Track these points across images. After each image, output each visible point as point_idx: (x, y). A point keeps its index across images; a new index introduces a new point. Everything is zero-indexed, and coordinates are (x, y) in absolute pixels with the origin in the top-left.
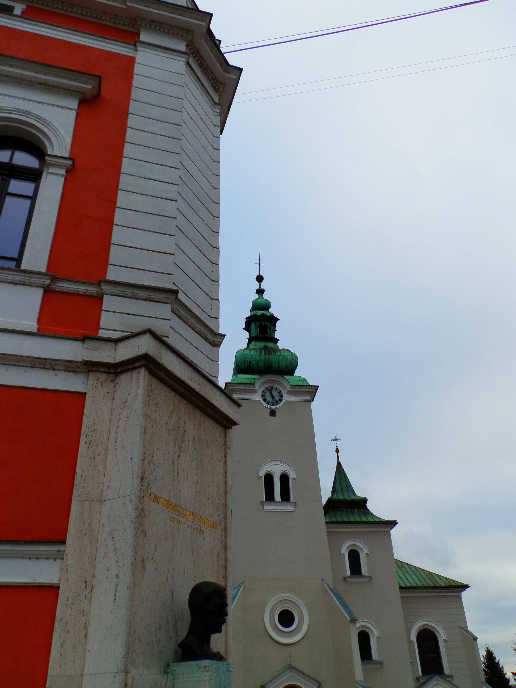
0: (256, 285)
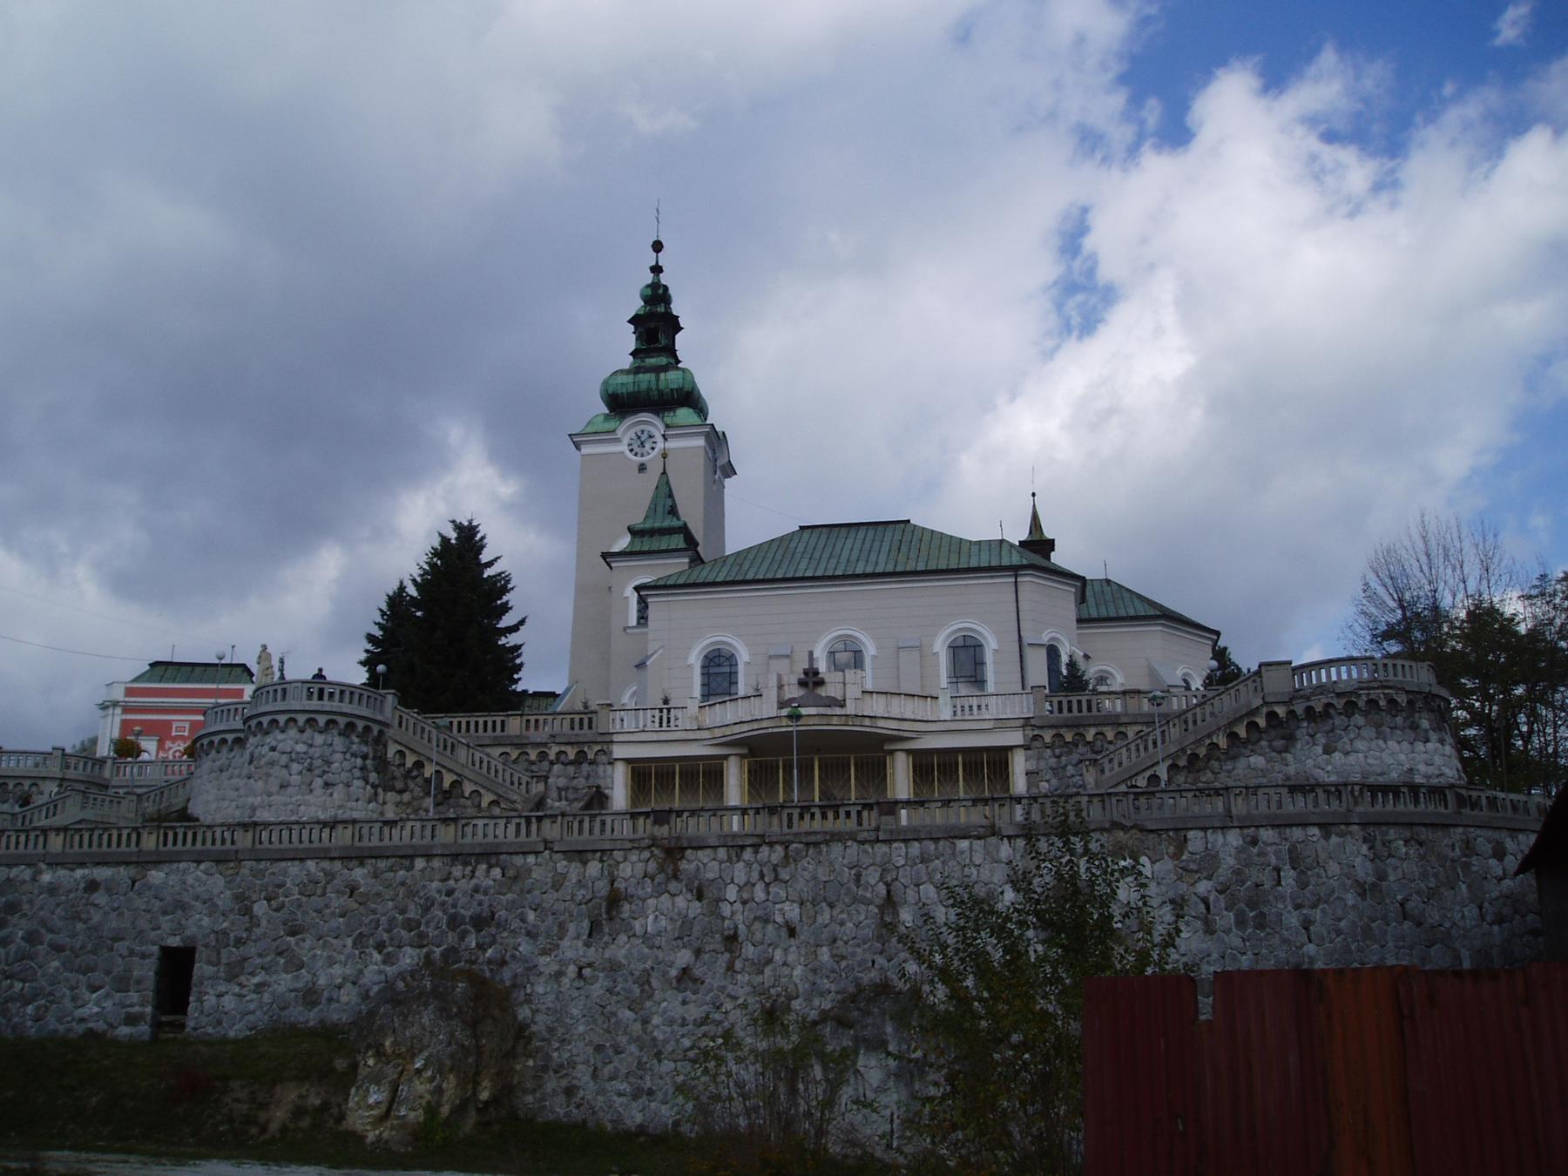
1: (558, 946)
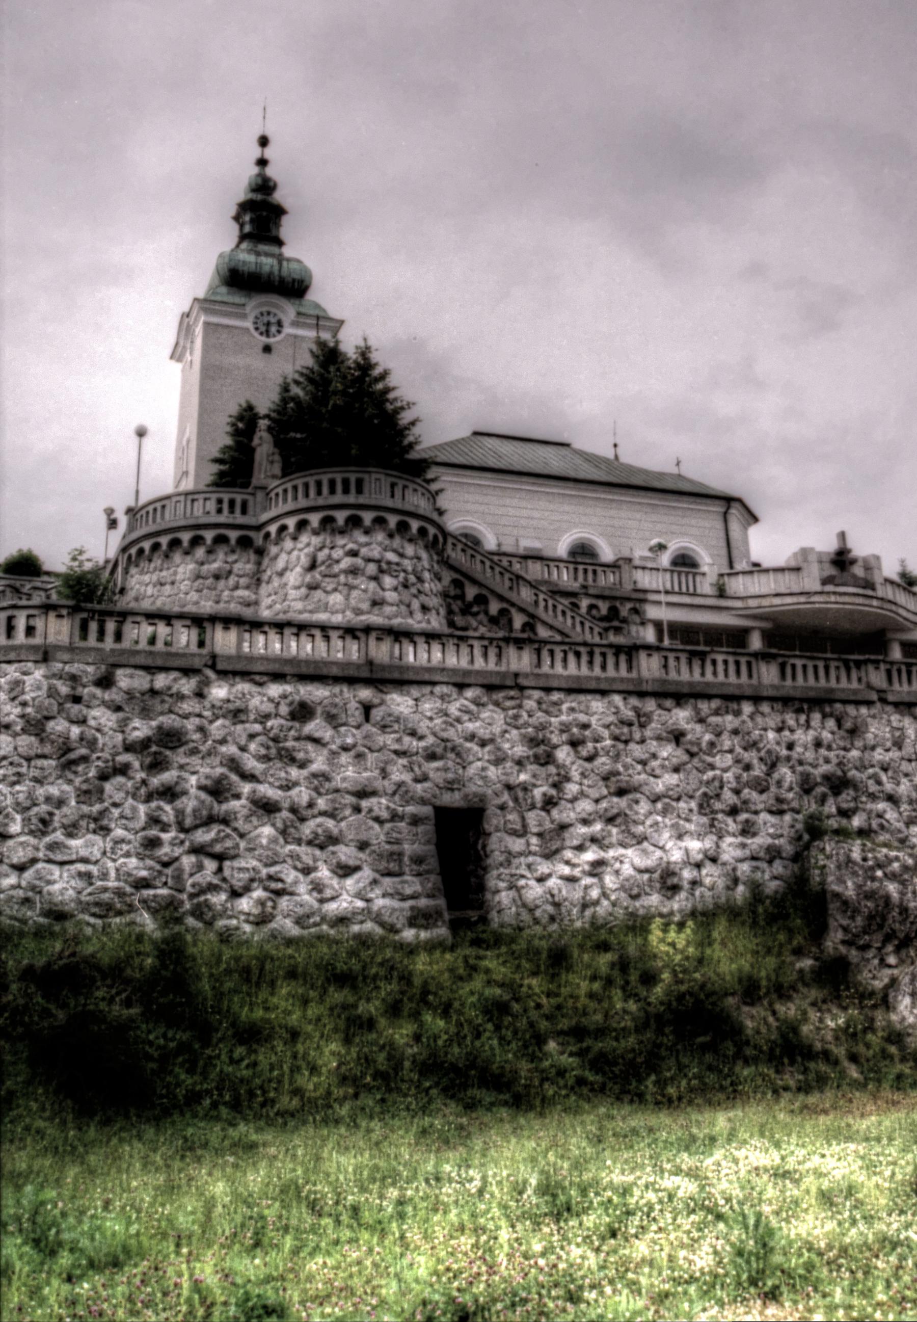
0: (256, 152)
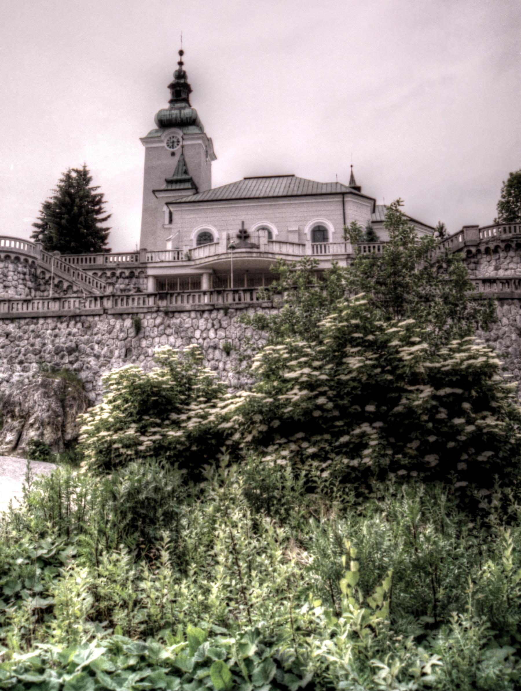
0: (178, 58)
1: (109, 362)
